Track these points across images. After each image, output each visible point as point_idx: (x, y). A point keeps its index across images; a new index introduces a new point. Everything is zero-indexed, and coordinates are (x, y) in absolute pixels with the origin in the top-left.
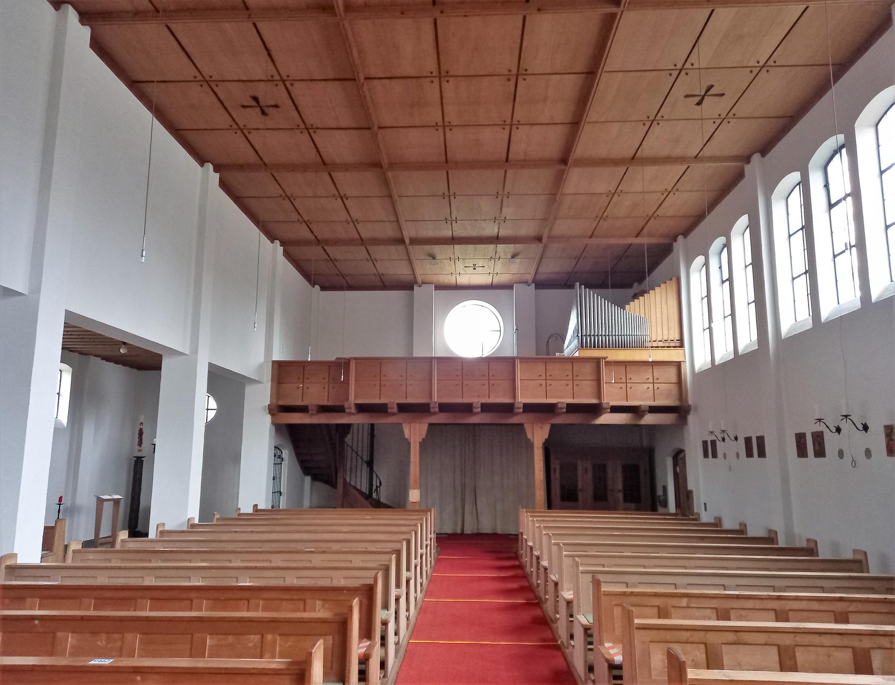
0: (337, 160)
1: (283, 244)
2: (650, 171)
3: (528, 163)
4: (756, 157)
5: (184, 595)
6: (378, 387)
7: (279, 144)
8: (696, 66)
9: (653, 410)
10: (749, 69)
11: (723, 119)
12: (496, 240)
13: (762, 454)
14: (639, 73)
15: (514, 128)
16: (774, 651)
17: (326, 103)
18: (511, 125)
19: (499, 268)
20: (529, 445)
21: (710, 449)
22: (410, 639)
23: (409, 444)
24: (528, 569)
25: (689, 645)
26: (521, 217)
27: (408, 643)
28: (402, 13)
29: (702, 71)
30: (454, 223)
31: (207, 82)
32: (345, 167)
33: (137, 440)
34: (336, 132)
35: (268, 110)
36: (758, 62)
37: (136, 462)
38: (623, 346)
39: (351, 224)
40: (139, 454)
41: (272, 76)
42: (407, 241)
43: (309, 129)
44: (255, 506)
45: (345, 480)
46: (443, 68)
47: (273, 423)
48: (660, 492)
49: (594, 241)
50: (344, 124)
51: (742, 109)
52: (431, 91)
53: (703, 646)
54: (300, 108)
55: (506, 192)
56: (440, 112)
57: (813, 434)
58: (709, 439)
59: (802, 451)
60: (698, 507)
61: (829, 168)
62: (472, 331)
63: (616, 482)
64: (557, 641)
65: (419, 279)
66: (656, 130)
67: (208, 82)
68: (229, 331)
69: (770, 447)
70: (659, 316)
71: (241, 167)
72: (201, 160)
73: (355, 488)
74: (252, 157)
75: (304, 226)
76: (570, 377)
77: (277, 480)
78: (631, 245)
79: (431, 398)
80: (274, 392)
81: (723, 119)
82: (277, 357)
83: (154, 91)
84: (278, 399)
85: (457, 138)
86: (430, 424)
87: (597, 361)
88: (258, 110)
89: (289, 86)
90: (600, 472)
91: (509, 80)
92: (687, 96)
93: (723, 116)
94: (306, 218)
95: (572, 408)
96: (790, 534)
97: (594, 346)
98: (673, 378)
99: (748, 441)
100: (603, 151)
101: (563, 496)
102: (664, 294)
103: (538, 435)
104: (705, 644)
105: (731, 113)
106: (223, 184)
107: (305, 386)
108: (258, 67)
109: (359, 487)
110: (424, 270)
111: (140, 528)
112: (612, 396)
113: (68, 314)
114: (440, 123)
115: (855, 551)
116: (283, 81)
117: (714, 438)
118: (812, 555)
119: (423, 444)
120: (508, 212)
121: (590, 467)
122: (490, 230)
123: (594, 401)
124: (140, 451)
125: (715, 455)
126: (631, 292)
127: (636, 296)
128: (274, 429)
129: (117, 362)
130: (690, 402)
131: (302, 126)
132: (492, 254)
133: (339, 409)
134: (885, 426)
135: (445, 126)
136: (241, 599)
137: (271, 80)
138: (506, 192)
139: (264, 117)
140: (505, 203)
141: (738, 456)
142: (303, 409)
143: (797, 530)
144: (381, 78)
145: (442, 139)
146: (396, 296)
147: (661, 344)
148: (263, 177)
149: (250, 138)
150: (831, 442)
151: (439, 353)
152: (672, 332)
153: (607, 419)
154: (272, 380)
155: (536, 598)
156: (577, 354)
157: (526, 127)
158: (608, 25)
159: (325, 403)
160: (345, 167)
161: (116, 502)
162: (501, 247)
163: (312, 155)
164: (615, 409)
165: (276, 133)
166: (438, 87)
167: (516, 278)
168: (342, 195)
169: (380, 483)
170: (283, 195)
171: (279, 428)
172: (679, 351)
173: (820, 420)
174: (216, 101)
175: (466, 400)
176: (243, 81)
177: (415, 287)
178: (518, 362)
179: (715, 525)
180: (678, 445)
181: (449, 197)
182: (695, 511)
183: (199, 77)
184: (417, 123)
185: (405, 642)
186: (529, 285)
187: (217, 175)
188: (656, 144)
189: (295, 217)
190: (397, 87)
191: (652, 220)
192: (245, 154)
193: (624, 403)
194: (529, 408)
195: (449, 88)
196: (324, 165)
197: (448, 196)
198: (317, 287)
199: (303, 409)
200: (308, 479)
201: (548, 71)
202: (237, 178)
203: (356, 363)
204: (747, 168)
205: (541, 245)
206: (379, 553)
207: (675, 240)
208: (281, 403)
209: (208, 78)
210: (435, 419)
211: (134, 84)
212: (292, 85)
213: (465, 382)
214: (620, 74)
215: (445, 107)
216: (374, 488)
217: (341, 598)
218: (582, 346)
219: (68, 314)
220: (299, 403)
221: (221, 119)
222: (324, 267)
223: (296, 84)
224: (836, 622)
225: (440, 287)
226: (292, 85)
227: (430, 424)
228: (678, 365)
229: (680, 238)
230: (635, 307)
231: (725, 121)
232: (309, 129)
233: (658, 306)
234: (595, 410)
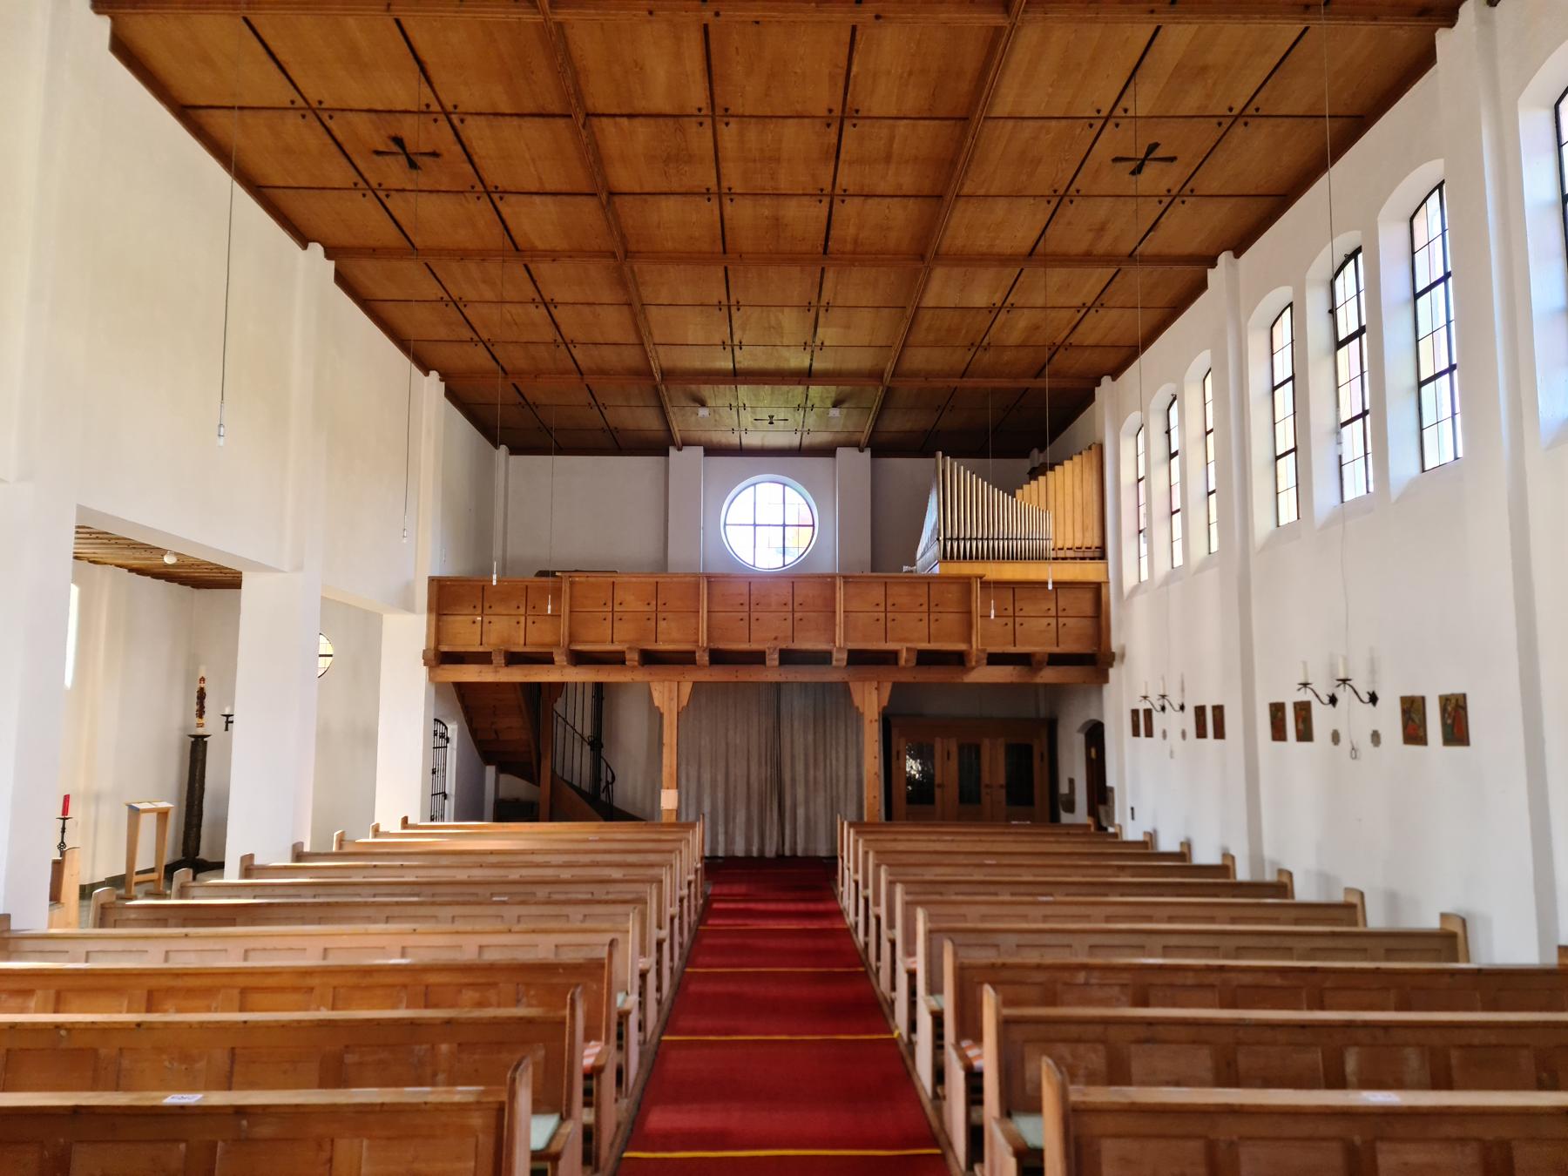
0: (540, 245)
2: (1057, 275)
3: (860, 256)
7: (438, 216)
8: (1131, 113)
9: (1056, 660)
10: (1215, 121)
11: (1173, 198)
12: (806, 377)
13: (1220, 733)
14: (1040, 122)
15: (837, 201)
17: (524, 152)
18: (832, 196)
19: (812, 419)
20: (859, 716)
21: (1142, 723)
22: (662, 1034)
23: (661, 715)
24: (850, 919)
26: (851, 339)
27: (660, 1041)
28: (651, 13)
29: (1140, 122)
30: (737, 349)
31: (314, 111)
32: (553, 256)
33: (196, 707)
34: (537, 199)
35: (420, 160)
36: (1231, 109)
37: (194, 745)
38: (1012, 557)
39: (563, 347)
40: (200, 731)
41: (428, 106)
42: (658, 377)
43: (492, 194)
44: (405, 820)
45: (553, 772)
46: (718, 101)
47: (431, 679)
48: (1064, 789)
49: (968, 383)
50: (549, 187)
51: (1211, 181)
52: (699, 139)
54: (476, 159)
55: (823, 302)
56: (714, 172)
57: (1445, 701)
58: (1142, 706)
59: (1278, 733)
60: (1120, 815)
61: (1561, 106)
62: (768, 524)
63: (994, 767)
64: (891, 1032)
65: (678, 437)
66: (1068, 211)
67: (315, 111)
68: (338, 501)
71: (374, 252)
72: (303, 240)
73: (571, 785)
74: (390, 236)
75: (481, 349)
76: (925, 607)
77: (440, 774)
81: (1173, 198)
83: (221, 123)
85: (743, 214)
87: (965, 582)
88: (402, 159)
89: (456, 121)
90: (970, 756)
91: (828, 125)
92: (1116, 160)
93: (1174, 192)
94: (485, 337)
95: (926, 658)
96: (1256, 859)
98: (1087, 607)
99: (1200, 711)
100: (982, 243)
101: (910, 803)
102: (1078, 470)
103: (870, 700)
105: (1188, 186)
106: (342, 279)
107: (486, 619)
108: (401, 90)
109: (576, 783)
110: (686, 420)
111: (204, 854)
113: (81, 509)
114: (714, 188)
115: (1348, 891)
116: (447, 115)
117: (1148, 706)
118: (1285, 896)
120: (827, 334)
121: (954, 749)
122: (797, 360)
123: (962, 647)
124: (201, 725)
125: (1149, 734)
126: (1026, 464)
127: (1034, 474)
128: (437, 692)
129: (156, 575)
131: (479, 187)
132: (800, 400)
134: (1404, 700)
135: (721, 194)
137: (427, 111)
138: (823, 302)
139: (414, 172)
140: (821, 320)
141: (1184, 735)
142: (483, 658)
143: (1269, 852)
144: (614, 116)
145: (717, 212)
147: (1070, 554)
148: (412, 269)
150: (1322, 718)
152: (1088, 534)
153: (985, 674)
154: (430, 610)
155: (863, 965)
156: (937, 570)
157: (857, 200)
158: (995, 47)
160: (553, 256)
161: (163, 815)
162: (815, 391)
163: (495, 237)
164: (995, 659)
165: (434, 196)
166: (709, 133)
167: (841, 437)
168: (547, 299)
169: (613, 778)
170: (446, 297)
171: (439, 688)
172: (1098, 565)
174: (330, 141)
175: (755, 646)
176: (376, 111)
177: (672, 451)
178: (839, 582)
179: (1144, 844)
180: (1094, 716)
181: (729, 307)
182: (1117, 821)
183: (300, 102)
184: (675, 187)
185: (655, 1041)
186: (861, 451)
187: (331, 265)
188: (1073, 233)
189: (466, 334)
190: (642, 129)
191: (1062, 350)
192: (380, 231)
193: (1011, 649)
194: (858, 658)
195: (729, 134)
196: (516, 249)
197: (728, 307)
198: (503, 448)
201: (894, 113)
202: (368, 272)
206: (614, 902)
209: (315, 105)
211: (186, 113)
212: (462, 121)
213: (754, 616)
215: (723, 165)
216: (603, 784)
217: (555, 980)
218: (945, 557)
219: (81, 509)
221: (339, 173)
222: (515, 414)
223: (469, 120)
225: (712, 450)
226: (462, 121)
230: (1031, 491)
231: (1178, 200)
232: (492, 194)
234: (958, 660)
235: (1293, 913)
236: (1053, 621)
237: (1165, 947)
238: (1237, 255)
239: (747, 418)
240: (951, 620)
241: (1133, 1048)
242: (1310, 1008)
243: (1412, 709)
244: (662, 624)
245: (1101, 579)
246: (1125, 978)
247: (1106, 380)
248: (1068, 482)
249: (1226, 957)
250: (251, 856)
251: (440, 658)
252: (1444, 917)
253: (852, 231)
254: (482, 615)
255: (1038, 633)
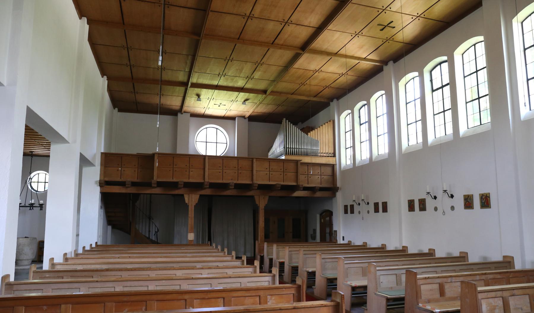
1: (108, 79)
4: (391, 63)
5: (180, 297)
6: (171, 172)
9: (322, 189)
10: (411, 16)
16: (527, 297)
20: (186, 206)
21: (349, 210)
25: (496, 299)
38: (306, 154)
48: (310, 232)
53: (501, 298)
57: (378, 212)
59: (346, 212)
61: (433, 72)
62: (211, 142)
69: (405, 206)
70: (324, 140)
76: (282, 170)
78: (310, 101)
79: (204, 179)
80: (102, 172)
82: (102, 151)
84: (105, 177)
86: (201, 196)
87: (297, 162)
97: (292, 154)
103: (262, 202)
104: (502, 297)
112: (303, 181)
119: (196, 206)
120: (257, 75)
123: (294, 184)
130: (339, 185)
133: (149, 185)
136: (218, 298)
141: (368, 212)
146: (168, 119)
147: (325, 155)
149: (122, 4)
150: (430, 203)
151: (191, 152)
152: (330, 148)
153: (298, 194)
156: (283, 158)
159: (136, 180)
164: (305, 189)
172: (334, 158)
173: (428, 193)
175: (175, 180)
177: (179, 114)
179: (364, 246)
180: (327, 208)
198: (117, 109)
199: (122, 184)
200: (110, 227)
203: (159, 157)
204: (331, 103)
205: (264, 96)
207: (332, 101)
208: (107, 179)
210: (273, 194)
213: (224, 171)
214: (356, 5)
220: (118, 179)
224: (486, 286)
227: (201, 196)
228: (333, 166)
229: (335, 100)
230: (312, 134)
233: (324, 135)
234: (293, 188)
235: (436, 261)
236: (320, 177)
237: (495, 267)
238: (338, 100)
239: (212, 102)
240: (291, 175)
241: (510, 297)
242: (507, 284)
243: (376, 205)
244: (191, 173)
245: (334, 163)
246: (461, 279)
247: (335, 100)
248: (324, 131)
249: (458, 272)
250: (53, 259)
251: (103, 184)
252: (430, 250)
253: (286, 36)
254: (121, 167)
255: (316, 180)
